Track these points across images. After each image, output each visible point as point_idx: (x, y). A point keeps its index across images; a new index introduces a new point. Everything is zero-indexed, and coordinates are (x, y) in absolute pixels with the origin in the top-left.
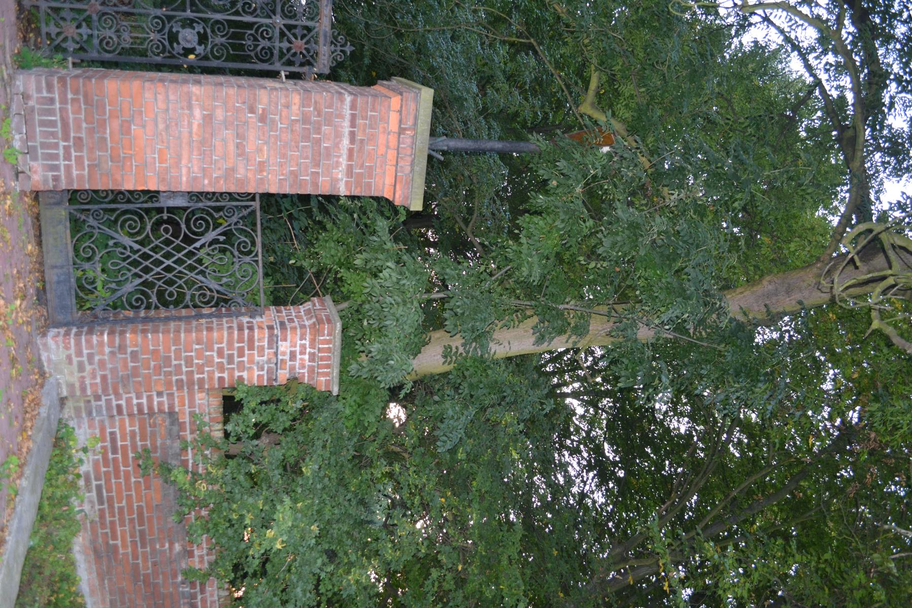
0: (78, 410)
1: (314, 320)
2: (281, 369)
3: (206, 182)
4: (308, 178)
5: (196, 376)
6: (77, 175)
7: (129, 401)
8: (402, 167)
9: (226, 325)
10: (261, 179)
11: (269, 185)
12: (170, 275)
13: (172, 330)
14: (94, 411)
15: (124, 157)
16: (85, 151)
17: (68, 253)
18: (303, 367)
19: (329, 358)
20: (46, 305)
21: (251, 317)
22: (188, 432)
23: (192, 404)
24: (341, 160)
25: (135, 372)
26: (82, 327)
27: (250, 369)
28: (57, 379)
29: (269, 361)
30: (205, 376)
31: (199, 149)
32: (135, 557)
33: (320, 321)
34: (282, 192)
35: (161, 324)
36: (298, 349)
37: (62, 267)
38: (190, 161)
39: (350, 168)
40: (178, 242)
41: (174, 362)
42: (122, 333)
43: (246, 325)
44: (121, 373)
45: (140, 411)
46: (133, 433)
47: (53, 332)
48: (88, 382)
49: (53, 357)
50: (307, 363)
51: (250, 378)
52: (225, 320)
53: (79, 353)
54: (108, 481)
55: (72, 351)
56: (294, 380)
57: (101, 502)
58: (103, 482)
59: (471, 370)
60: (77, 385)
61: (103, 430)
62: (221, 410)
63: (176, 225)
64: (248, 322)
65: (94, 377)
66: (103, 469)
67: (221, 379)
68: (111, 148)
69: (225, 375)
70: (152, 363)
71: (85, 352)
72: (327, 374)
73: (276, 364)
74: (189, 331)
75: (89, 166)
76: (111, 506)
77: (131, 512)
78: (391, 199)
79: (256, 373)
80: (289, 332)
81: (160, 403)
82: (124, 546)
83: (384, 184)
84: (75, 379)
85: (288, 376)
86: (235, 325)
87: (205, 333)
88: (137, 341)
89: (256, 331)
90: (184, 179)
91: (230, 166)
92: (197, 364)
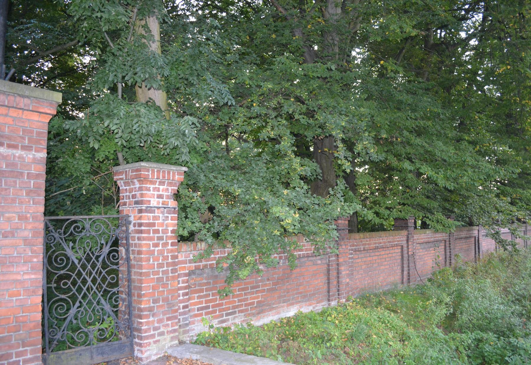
0: (185, 332)
1: (135, 181)
2: (168, 205)
3: (35, 260)
4: (32, 182)
5: (170, 260)
6: (31, 354)
7: (181, 302)
8: (25, 105)
9: (136, 241)
10: (33, 218)
11: (38, 212)
12: (99, 280)
13: (139, 277)
14: (185, 322)
15: (16, 322)
16: (11, 351)
17: (82, 350)
18: (167, 190)
19: (164, 172)
20: (118, 360)
21: (130, 224)
22: (201, 264)
23: (184, 262)
24: (17, 155)
25: (165, 300)
26: (134, 335)
27: (167, 226)
28: (168, 348)
29: (163, 213)
30: (170, 255)
31: (9, 266)
32: (263, 291)
33: (138, 177)
34: (43, 202)
35: (133, 284)
36: (156, 193)
37: (92, 352)
38: (18, 273)
39: (24, 148)
40: (74, 275)
41: (161, 275)
42: (140, 310)
43: (137, 228)
44: (166, 309)
45: (187, 294)
46: (199, 297)
47: (136, 353)
48: (170, 329)
49: (155, 352)
50: (165, 187)
51: (174, 225)
52: (131, 242)
53: (153, 336)
54: (224, 310)
55: (151, 341)
56: (177, 196)
57: (234, 313)
58: (224, 313)
59: (179, 72)
60: (172, 335)
61: (196, 316)
62: (189, 243)
63: (61, 278)
64: (134, 226)
65: (168, 325)
66: (218, 313)
67: (173, 244)
68: (8, 332)
69: (170, 242)
70: (161, 289)
71: (152, 332)
72: (174, 174)
73: (165, 208)
74: (141, 267)
75: (23, 347)
76: (237, 307)
77: (241, 295)
78: (51, 117)
79: (170, 221)
80: (145, 199)
81: (183, 283)
82: (257, 297)
83: (38, 121)
84: (168, 337)
85: (172, 200)
86: (137, 235)
87: (143, 256)
88: (147, 300)
89: (143, 221)
90: (33, 276)
91: (22, 242)
92: (162, 260)
